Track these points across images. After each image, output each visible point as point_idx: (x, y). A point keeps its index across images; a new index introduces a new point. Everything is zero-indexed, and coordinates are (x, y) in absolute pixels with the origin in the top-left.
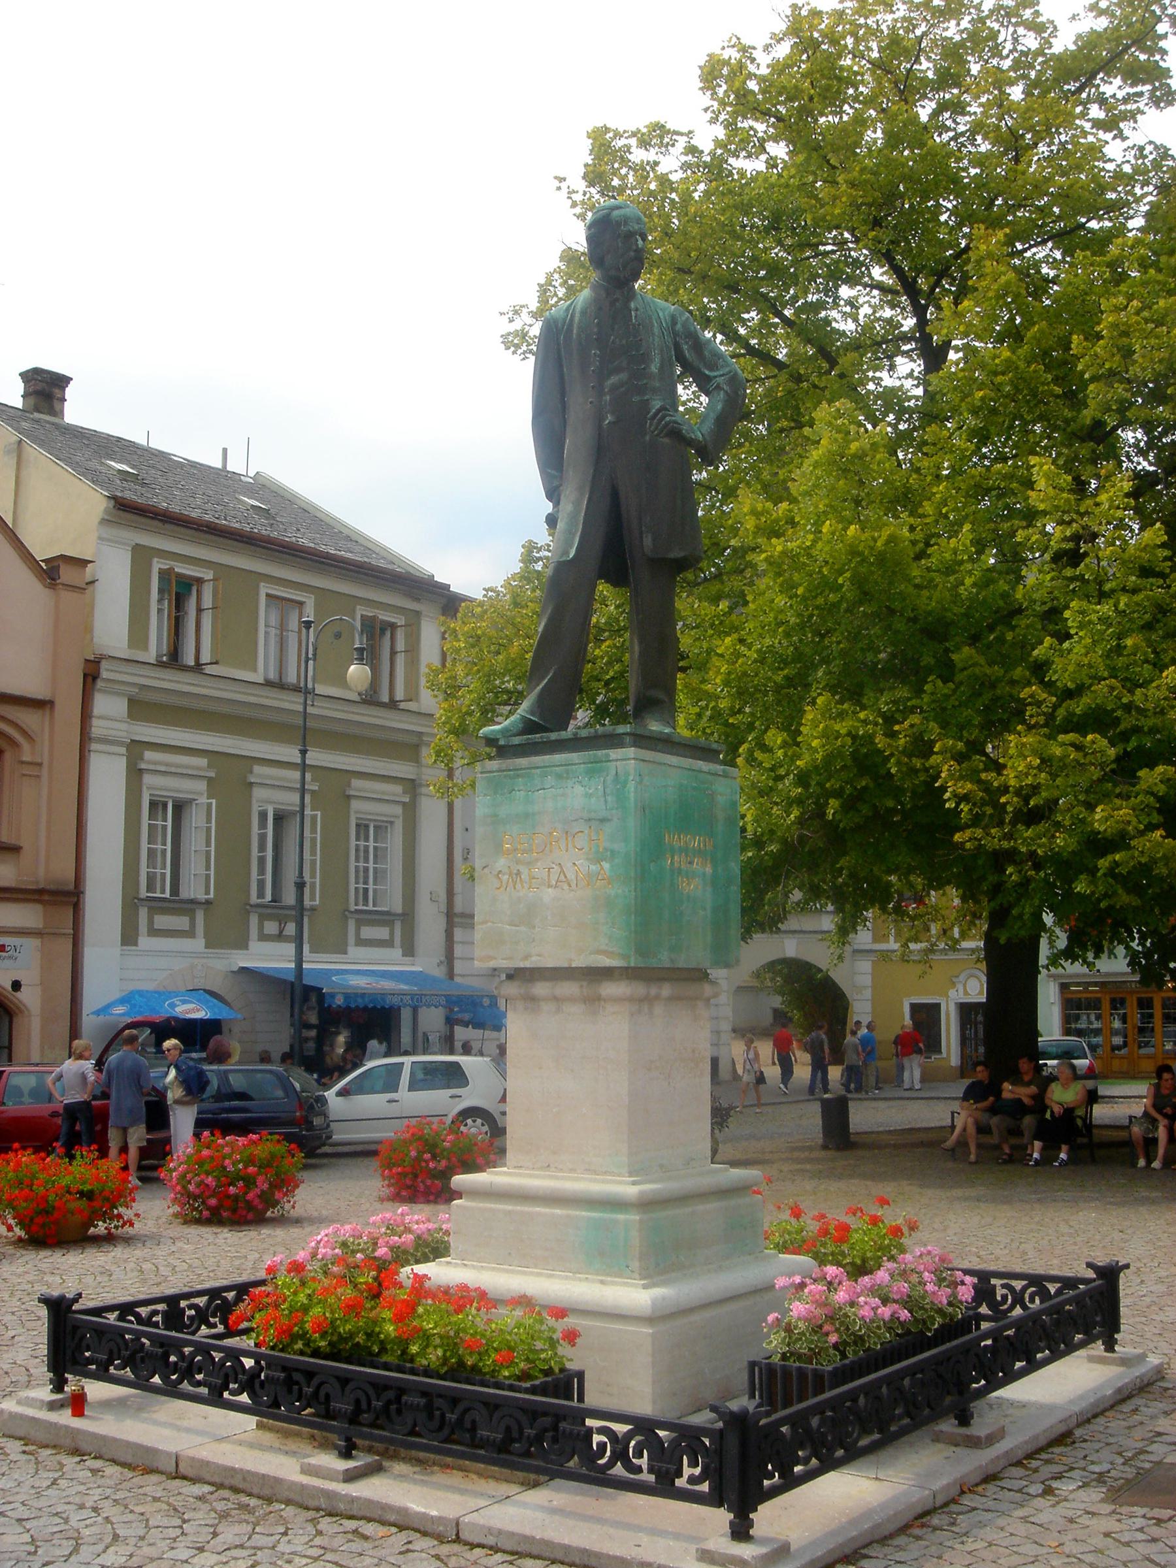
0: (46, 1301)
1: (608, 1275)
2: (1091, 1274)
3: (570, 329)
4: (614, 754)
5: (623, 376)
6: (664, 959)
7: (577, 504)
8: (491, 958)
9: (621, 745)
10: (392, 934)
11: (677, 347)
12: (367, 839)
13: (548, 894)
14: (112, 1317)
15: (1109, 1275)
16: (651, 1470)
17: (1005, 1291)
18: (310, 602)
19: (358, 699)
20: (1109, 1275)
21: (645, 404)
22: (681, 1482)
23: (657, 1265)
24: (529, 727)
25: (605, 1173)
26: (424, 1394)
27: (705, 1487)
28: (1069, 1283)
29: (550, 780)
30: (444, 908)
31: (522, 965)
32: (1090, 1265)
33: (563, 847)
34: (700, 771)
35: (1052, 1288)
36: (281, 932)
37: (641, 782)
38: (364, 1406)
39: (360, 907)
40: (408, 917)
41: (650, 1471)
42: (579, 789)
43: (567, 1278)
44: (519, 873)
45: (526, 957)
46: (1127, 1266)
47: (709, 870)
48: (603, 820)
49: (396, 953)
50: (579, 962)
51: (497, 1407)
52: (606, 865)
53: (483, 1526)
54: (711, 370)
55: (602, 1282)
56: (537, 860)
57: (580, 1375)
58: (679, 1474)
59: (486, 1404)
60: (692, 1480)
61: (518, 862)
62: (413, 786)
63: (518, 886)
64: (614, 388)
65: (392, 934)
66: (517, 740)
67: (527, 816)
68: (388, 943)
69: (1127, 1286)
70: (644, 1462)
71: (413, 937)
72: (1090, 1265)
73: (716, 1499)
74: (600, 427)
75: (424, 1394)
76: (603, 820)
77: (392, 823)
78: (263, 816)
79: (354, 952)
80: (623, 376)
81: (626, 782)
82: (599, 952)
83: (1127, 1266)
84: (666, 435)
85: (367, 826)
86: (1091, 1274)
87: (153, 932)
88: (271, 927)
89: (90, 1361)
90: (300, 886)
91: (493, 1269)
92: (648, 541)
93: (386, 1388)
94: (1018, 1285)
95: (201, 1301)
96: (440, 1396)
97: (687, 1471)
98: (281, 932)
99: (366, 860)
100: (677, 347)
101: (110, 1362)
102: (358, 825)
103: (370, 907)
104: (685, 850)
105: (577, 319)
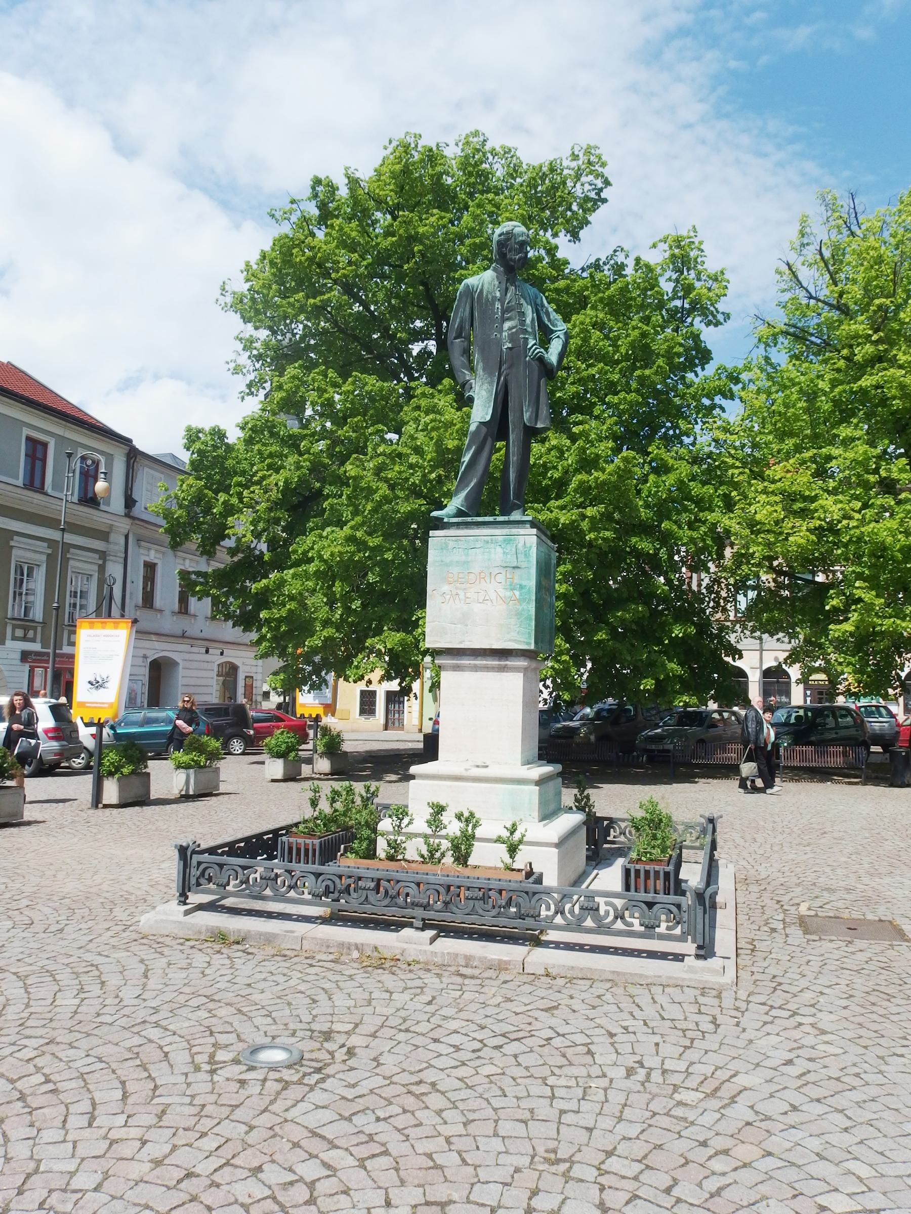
3: (482, 290)
4: (522, 531)
13: (477, 608)
24: (460, 513)
42: (499, 550)
45: (461, 643)
52: (517, 593)
59: (527, 893)
62: (103, 555)
63: (457, 601)
64: (510, 329)
82: (510, 640)
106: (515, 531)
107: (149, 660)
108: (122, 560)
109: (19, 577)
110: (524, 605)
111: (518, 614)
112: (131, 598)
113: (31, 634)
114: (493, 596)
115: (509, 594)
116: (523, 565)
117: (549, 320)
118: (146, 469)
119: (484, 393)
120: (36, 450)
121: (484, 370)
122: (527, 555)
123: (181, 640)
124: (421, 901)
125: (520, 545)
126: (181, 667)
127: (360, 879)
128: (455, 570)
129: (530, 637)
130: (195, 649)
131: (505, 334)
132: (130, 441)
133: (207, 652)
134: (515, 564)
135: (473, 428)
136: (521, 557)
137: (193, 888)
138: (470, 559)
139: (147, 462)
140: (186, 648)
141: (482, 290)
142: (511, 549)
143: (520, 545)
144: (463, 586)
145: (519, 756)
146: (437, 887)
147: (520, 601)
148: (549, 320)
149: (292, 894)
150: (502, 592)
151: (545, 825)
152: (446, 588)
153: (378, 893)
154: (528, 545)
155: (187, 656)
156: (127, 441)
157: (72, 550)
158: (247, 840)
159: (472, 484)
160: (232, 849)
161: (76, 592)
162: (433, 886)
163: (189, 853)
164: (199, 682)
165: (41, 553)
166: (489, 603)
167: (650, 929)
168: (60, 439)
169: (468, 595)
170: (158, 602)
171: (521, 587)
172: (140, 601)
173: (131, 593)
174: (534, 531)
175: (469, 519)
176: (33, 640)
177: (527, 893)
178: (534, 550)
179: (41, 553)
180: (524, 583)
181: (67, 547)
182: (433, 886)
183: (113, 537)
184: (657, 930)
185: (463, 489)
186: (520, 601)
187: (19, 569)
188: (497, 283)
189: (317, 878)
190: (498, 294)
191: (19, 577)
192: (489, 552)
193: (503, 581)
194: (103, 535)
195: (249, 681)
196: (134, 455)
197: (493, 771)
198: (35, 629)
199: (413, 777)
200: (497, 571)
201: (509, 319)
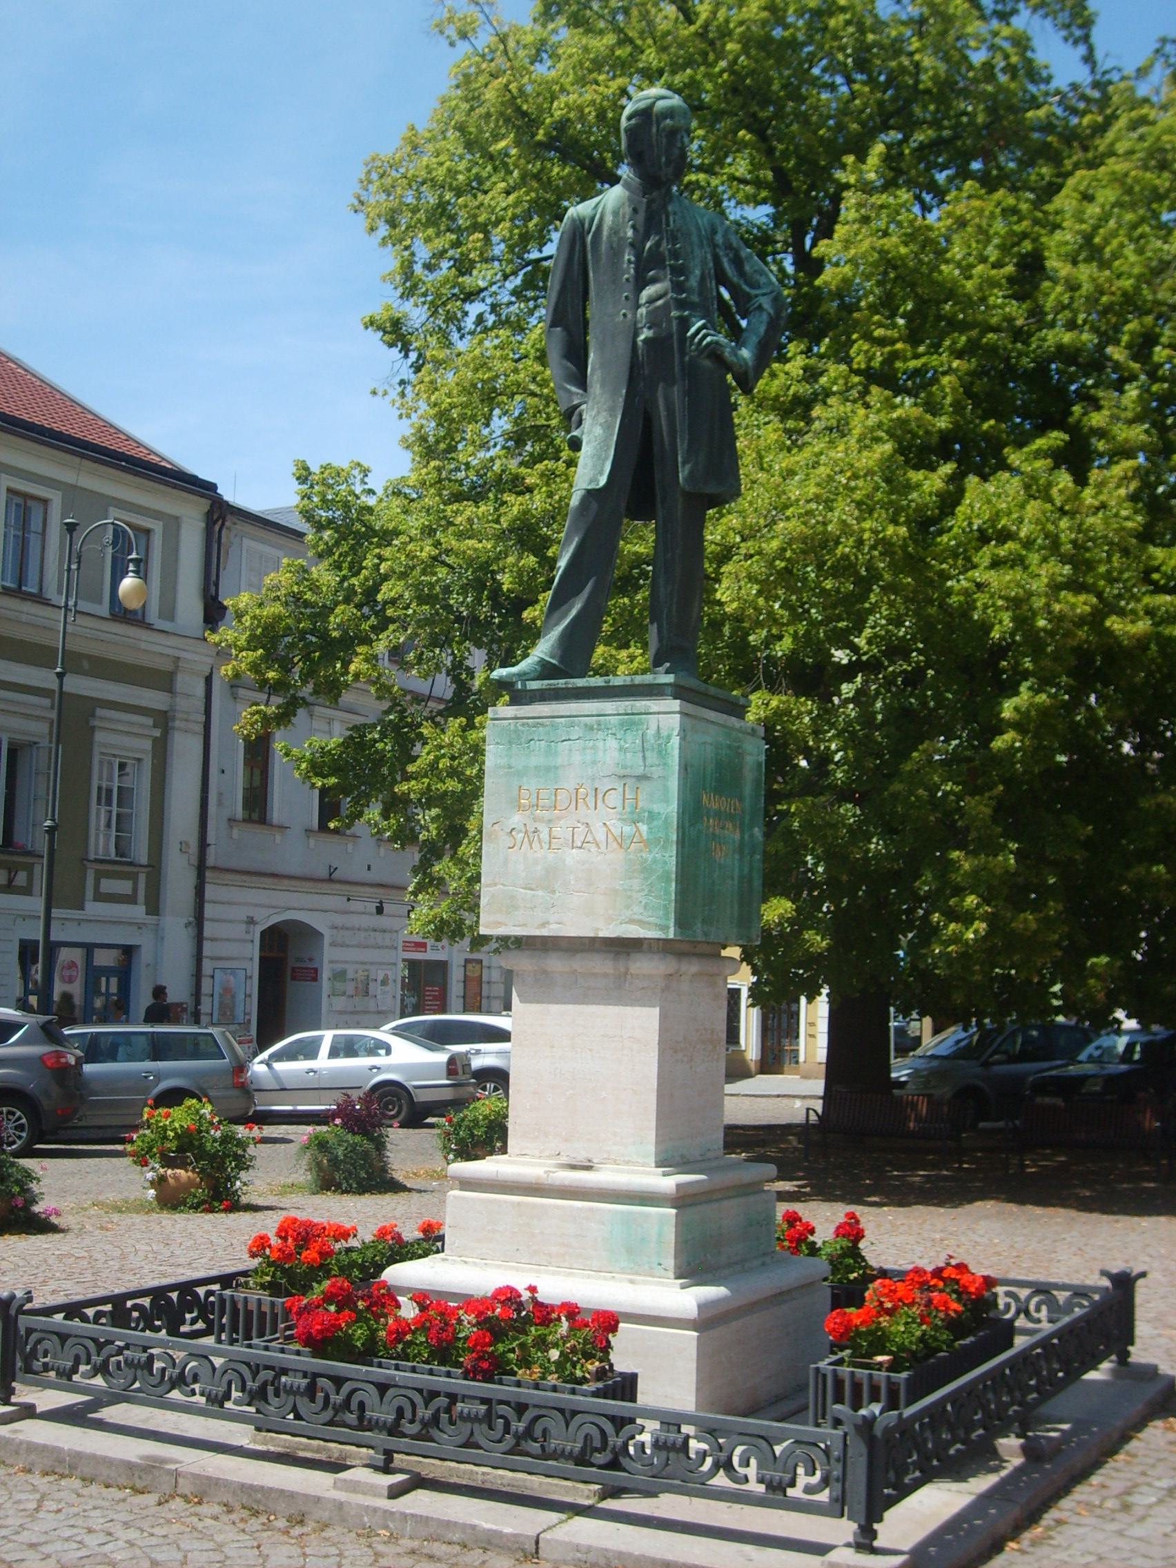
0: (371, 323)
1: (637, 1273)
2: (1106, 1283)
7: (607, 427)
8: (499, 924)
10: (135, 889)
11: (717, 260)
13: (572, 857)
14: (59, 1317)
15: (1124, 1284)
16: (761, 1481)
17: (1008, 1300)
18: (56, 498)
20: (1124, 1284)
22: (794, 1493)
24: (546, 671)
25: (628, 1163)
26: (484, 1401)
27: (824, 1496)
28: (1080, 1292)
29: (576, 732)
31: (537, 933)
32: (1104, 1273)
33: (592, 805)
34: (732, 728)
35: (1062, 1296)
36: (10, 881)
38: (408, 1414)
40: (155, 868)
41: (760, 1481)
42: (612, 743)
43: (589, 1277)
45: (543, 925)
46: (1143, 1275)
47: (737, 836)
48: (643, 778)
49: (138, 911)
50: (607, 932)
51: (575, 1413)
52: (644, 828)
53: (567, 1543)
54: (752, 286)
55: (632, 1282)
56: (559, 818)
58: (792, 1484)
59: (562, 1411)
60: (809, 1490)
61: (535, 820)
62: (164, 720)
63: (536, 845)
64: (651, 301)
65: (135, 889)
66: (534, 685)
67: (548, 769)
68: (131, 899)
69: (1141, 1291)
70: (752, 1471)
71: (158, 889)
72: (1104, 1273)
73: (838, 1508)
74: (634, 343)
75: (484, 1401)
76: (643, 778)
79: (94, 909)
81: (669, 737)
82: (631, 921)
83: (1143, 1275)
84: (709, 357)
86: (1106, 1283)
89: (46, 1368)
91: (499, 1267)
93: (434, 1394)
94: (1024, 1293)
95: (146, 1302)
96: (501, 1402)
97: (803, 1480)
98: (10, 881)
100: (717, 260)
101: (74, 1370)
104: (718, 814)
106: (641, 704)
107: (259, 929)
108: (200, 728)
110: (656, 853)
111: (646, 870)
112: (220, 803)
113: (21, 878)
114: (600, 835)
115: (628, 829)
116: (656, 772)
118: (246, 542)
119: (598, 431)
120: (24, 507)
121: (603, 386)
122: (662, 752)
123: (326, 887)
124: (383, 1417)
125: (651, 732)
126: (327, 941)
127: (285, 1372)
128: (531, 784)
129: (667, 914)
130: (355, 906)
132: (212, 487)
133: (380, 910)
134: (640, 771)
135: (575, 501)
136: (652, 757)
137: (19, 1374)
138: (559, 761)
139: (248, 528)
140: (337, 902)
142: (633, 740)
145: (652, 1148)
146: (410, 1393)
147: (647, 843)
149: (175, 1395)
150: (616, 827)
151: (683, 1287)
152: (516, 819)
153: (313, 1400)
154: (664, 733)
155: (339, 920)
156: (206, 489)
157: (100, 712)
158: (158, 1293)
159: (574, 612)
160: (119, 1309)
161: (109, 791)
162: (403, 1391)
163: (13, 1312)
165: (38, 718)
166: (593, 848)
167: (776, 1492)
168: (71, 490)
170: (277, 812)
171: (652, 816)
172: (239, 812)
173: (220, 794)
174: (675, 705)
175: (561, 683)
176: (27, 891)
177: (562, 1411)
178: (675, 741)
179: (38, 718)
180: (656, 808)
181: (90, 705)
182: (403, 1391)
183: (181, 681)
184: (790, 1492)
186: (647, 843)
188: (628, 210)
192: (594, 748)
193: (619, 805)
194: (164, 680)
195: (473, 971)
196: (220, 514)
197: (603, 1177)
198: (29, 869)
201: (654, 281)
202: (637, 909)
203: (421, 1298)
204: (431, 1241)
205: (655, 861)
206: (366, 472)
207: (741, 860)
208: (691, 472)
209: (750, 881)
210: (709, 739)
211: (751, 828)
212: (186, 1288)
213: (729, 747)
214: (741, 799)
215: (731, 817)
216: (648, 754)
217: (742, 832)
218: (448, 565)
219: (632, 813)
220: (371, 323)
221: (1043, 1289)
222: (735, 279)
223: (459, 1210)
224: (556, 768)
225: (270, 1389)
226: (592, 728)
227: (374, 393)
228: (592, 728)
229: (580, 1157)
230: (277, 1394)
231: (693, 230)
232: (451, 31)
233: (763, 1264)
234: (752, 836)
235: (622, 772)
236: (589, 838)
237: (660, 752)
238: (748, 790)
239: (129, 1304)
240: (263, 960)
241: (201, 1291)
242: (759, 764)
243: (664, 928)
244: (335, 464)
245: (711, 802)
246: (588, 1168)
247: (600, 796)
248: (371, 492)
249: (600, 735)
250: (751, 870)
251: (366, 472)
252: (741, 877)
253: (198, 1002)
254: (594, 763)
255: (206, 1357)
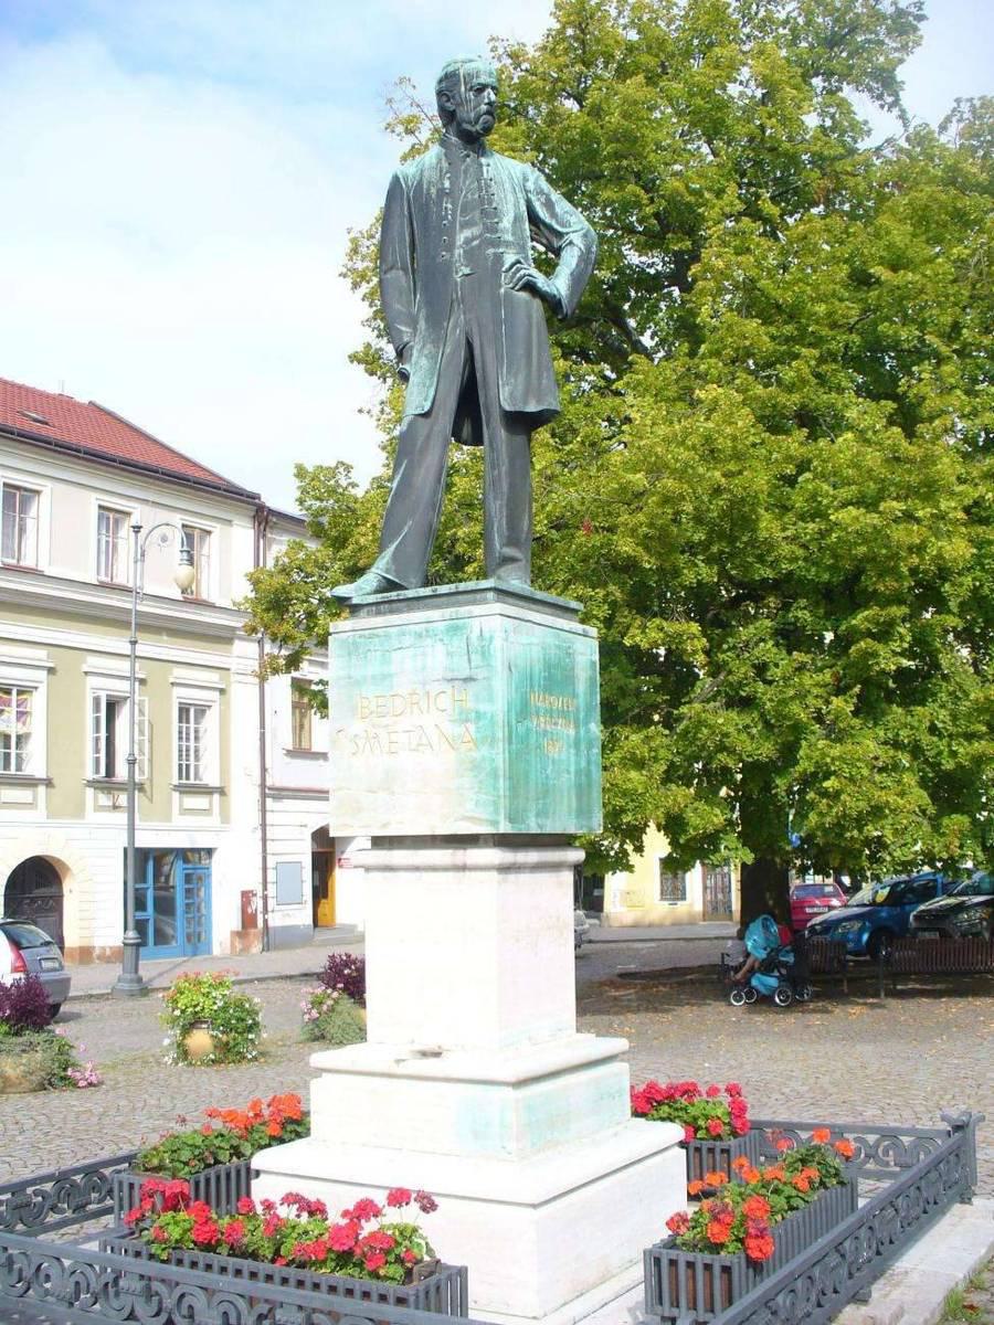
0: (353, 358)
4: (476, 610)
5: (476, 231)
6: (532, 826)
9: (485, 601)
10: (35, 798)
12: (188, 722)
19: (179, 597)
21: (499, 258)
23: (534, 1144)
28: (923, 1138)
29: (407, 641)
30: (259, 782)
35: (906, 1140)
37: (506, 640)
39: (184, 781)
42: (439, 646)
44: (376, 737)
45: (385, 826)
47: (572, 732)
54: (563, 226)
57: (462, 1273)
64: (468, 241)
67: (385, 677)
77: (209, 707)
78: (97, 701)
80: (476, 231)
85: (188, 711)
87: (185, 811)
88: (104, 799)
90: (132, 762)
92: (504, 394)
94: (871, 1138)
95: (48, 1187)
99: (188, 739)
102: (181, 710)
103: (192, 781)
105: (426, 174)
106: (464, 610)
109: (184, 763)
110: (485, 751)
111: (475, 767)
115: (460, 730)
116: (480, 674)
117: (553, 215)
119: (424, 362)
121: (427, 321)
125: (475, 635)
129: (496, 811)
131: (458, 252)
134: (466, 673)
141: (420, 183)
142: (458, 643)
143: (475, 635)
144: (384, 721)
148: (553, 215)
154: (486, 635)
158: (61, 1178)
164: (796, 1233)
169: (394, 737)
180: (482, 707)
185: (391, 542)
187: (184, 711)
188: (445, 165)
189: (132, 1312)
190: (447, 184)
191: (184, 763)
192: (424, 654)
199: (320, 1071)
200: (435, 688)
202: (470, 805)
203: (820, 924)
204: (292, 1125)
205: (484, 759)
206: (348, 468)
207: (577, 754)
208: (511, 394)
209: (589, 774)
210: (535, 640)
211: (586, 724)
212: (91, 1170)
213: (558, 647)
214: (574, 695)
215: (564, 714)
216: (473, 657)
217: (577, 727)
218: (792, 698)
219: (460, 713)
220: (353, 358)
221: (890, 1135)
222: (548, 220)
223: (324, 1101)
224: (390, 675)
225: (111, 1290)
226: (420, 636)
227: (360, 411)
228: (420, 636)
229: (431, 1046)
230: (117, 1294)
231: (505, 178)
232: (400, 129)
233: (616, 1134)
234: (588, 731)
235: (450, 676)
236: (424, 741)
237: (483, 653)
238: (581, 687)
239: (30, 1190)
240: (314, 855)
241: (107, 1172)
242: (594, 663)
243: (495, 823)
244: (325, 465)
245: (538, 701)
246: (437, 1055)
247: (432, 700)
248: (354, 485)
249: (429, 641)
250: (589, 763)
251: (348, 468)
252: (578, 773)
253: (265, 889)
254: (424, 668)
255: (58, 1259)
